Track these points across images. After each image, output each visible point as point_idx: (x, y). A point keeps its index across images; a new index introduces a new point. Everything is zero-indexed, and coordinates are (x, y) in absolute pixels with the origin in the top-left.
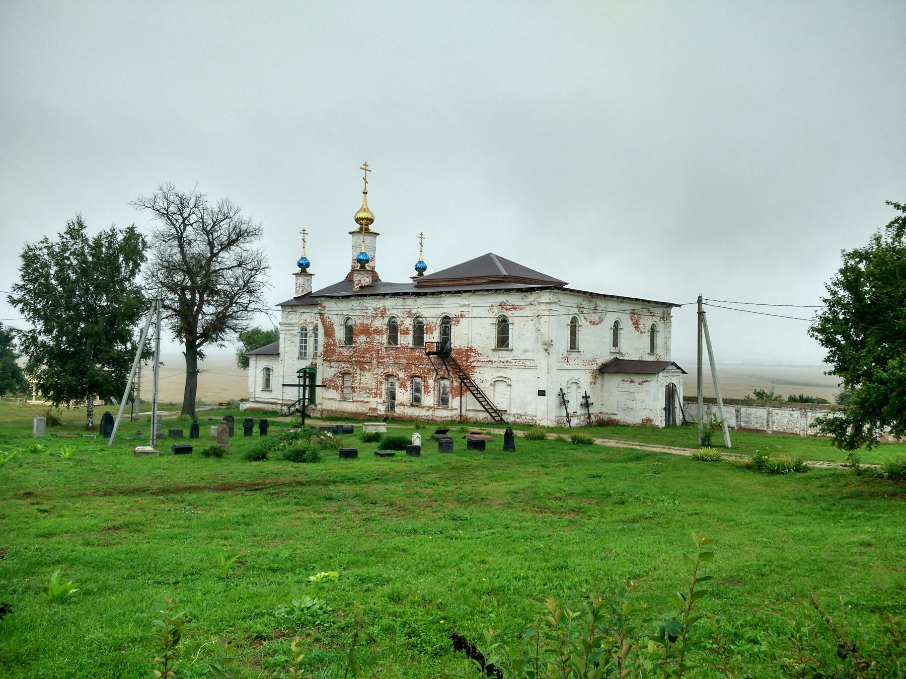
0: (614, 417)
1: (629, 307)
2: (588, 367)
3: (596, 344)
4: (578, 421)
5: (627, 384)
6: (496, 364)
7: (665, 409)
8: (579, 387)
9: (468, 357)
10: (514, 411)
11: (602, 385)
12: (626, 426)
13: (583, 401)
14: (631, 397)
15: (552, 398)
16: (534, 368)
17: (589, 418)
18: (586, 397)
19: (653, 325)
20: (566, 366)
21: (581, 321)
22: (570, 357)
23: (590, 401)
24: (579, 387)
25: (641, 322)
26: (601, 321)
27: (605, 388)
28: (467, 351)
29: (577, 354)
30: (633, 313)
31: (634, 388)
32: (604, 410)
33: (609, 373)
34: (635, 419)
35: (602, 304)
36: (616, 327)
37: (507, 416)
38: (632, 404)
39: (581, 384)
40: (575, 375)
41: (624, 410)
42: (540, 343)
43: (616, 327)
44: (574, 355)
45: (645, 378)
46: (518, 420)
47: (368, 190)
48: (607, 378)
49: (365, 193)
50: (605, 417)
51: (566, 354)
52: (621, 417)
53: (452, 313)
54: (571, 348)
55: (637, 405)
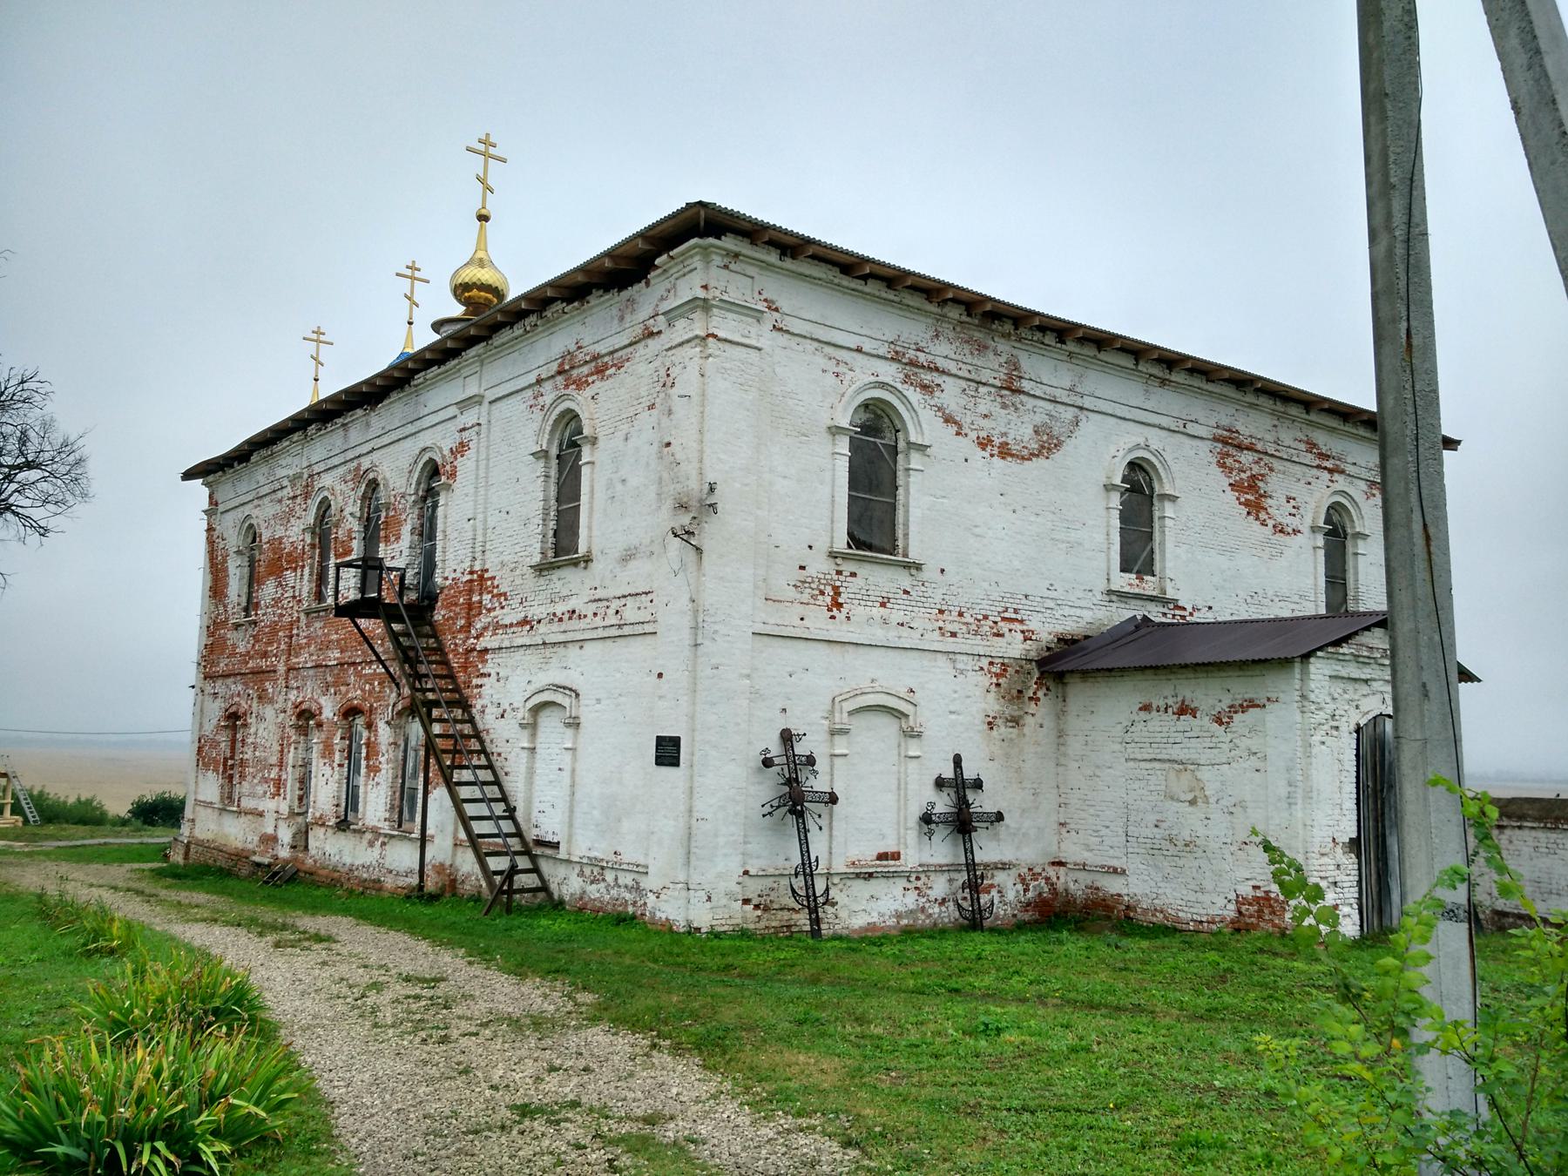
0: (1113, 886)
1: (1210, 414)
2: (977, 645)
3: (1016, 530)
4: (911, 900)
5: (1162, 725)
6: (545, 631)
7: (1354, 845)
8: (912, 734)
9: (472, 610)
10: (582, 845)
11: (1061, 734)
12: (1166, 930)
13: (944, 804)
14: (1180, 786)
15: (728, 783)
16: (645, 632)
17: (974, 886)
18: (959, 785)
19: (1335, 508)
20: (818, 621)
21: (921, 422)
22: (850, 588)
23: (982, 803)
24: (912, 734)
25: (1276, 486)
26: (1048, 444)
27: (1075, 745)
28: (470, 588)
29: (904, 579)
30: (1228, 443)
31: (1194, 739)
32: (1072, 851)
33: (1086, 674)
34: (1207, 891)
35: (1046, 371)
36: (1139, 491)
37: (562, 871)
38: (1190, 822)
39: (926, 716)
40: (886, 675)
41: (1154, 850)
42: (669, 504)
43: (1139, 491)
44: (875, 578)
45: (1241, 688)
46: (594, 891)
47: (491, 209)
48: (1079, 694)
49: (483, 218)
50: (1074, 884)
51: (820, 566)
52: (1140, 885)
53: (442, 441)
54: (855, 541)
55: (1214, 829)
